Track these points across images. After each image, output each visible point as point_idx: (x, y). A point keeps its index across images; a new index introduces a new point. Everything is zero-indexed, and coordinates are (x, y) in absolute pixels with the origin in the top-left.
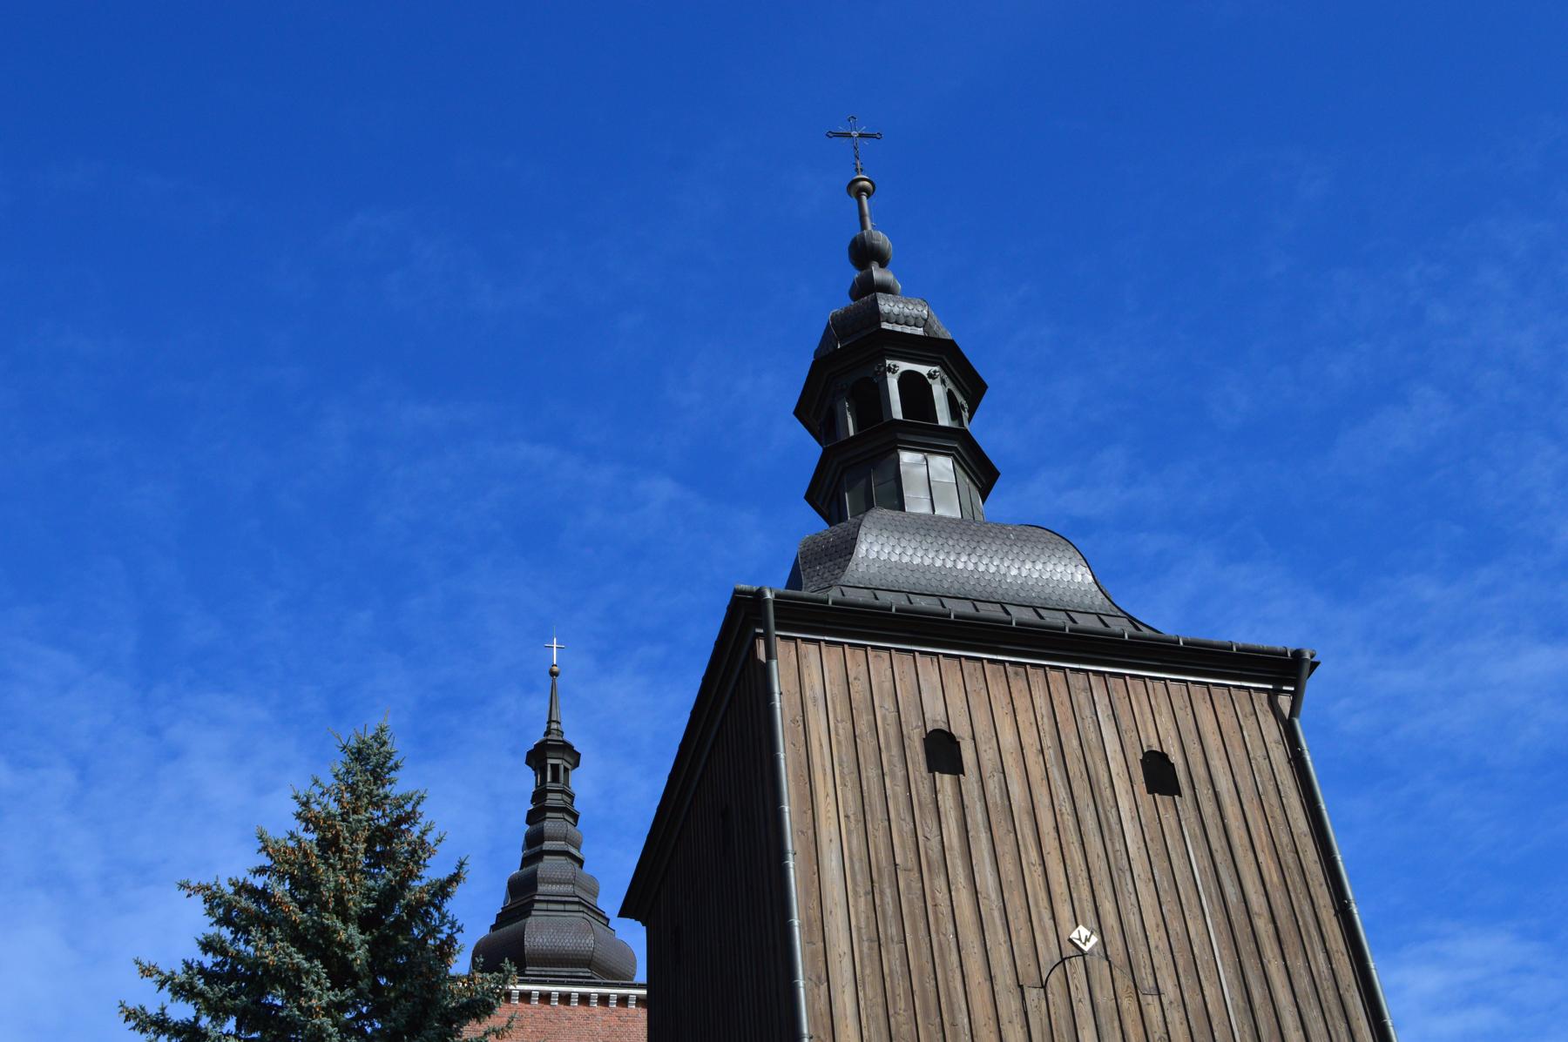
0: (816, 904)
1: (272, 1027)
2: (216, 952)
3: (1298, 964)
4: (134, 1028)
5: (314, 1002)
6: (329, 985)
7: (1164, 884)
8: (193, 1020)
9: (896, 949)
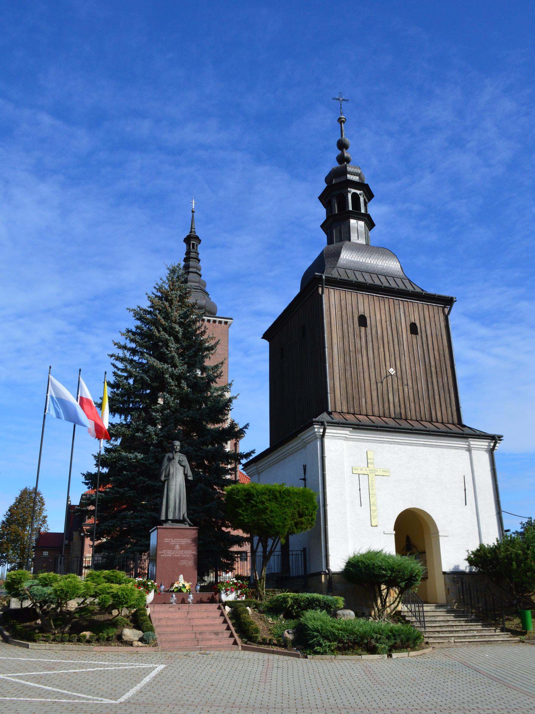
0: (331, 360)
3: (440, 380)
7: (412, 358)
9: (349, 372)
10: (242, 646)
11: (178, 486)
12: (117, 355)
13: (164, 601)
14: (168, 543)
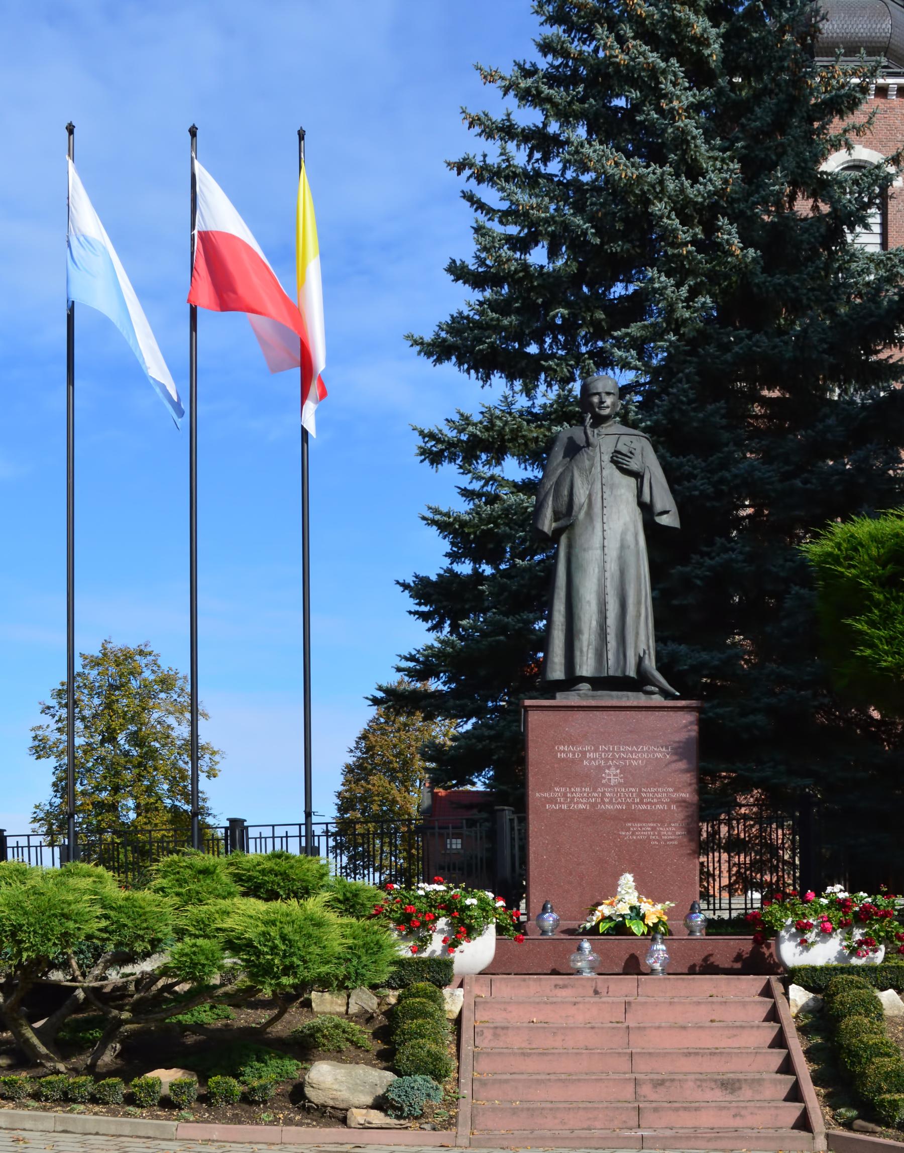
1: (625, 131)
2: (556, 53)
4: (480, 135)
5: (676, 104)
6: (687, 85)
8: (541, 125)
10: (828, 1136)
11: (613, 553)
12: (478, 161)
13: (551, 966)
14: (573, 761)
